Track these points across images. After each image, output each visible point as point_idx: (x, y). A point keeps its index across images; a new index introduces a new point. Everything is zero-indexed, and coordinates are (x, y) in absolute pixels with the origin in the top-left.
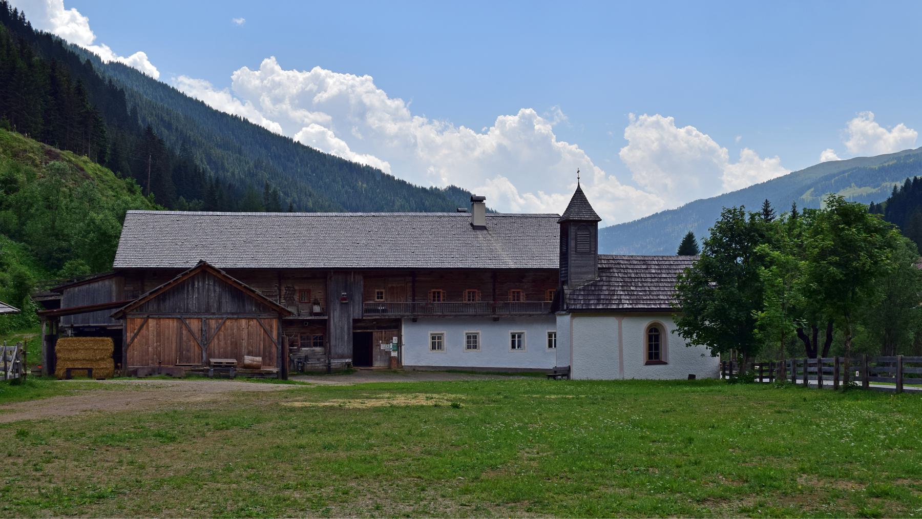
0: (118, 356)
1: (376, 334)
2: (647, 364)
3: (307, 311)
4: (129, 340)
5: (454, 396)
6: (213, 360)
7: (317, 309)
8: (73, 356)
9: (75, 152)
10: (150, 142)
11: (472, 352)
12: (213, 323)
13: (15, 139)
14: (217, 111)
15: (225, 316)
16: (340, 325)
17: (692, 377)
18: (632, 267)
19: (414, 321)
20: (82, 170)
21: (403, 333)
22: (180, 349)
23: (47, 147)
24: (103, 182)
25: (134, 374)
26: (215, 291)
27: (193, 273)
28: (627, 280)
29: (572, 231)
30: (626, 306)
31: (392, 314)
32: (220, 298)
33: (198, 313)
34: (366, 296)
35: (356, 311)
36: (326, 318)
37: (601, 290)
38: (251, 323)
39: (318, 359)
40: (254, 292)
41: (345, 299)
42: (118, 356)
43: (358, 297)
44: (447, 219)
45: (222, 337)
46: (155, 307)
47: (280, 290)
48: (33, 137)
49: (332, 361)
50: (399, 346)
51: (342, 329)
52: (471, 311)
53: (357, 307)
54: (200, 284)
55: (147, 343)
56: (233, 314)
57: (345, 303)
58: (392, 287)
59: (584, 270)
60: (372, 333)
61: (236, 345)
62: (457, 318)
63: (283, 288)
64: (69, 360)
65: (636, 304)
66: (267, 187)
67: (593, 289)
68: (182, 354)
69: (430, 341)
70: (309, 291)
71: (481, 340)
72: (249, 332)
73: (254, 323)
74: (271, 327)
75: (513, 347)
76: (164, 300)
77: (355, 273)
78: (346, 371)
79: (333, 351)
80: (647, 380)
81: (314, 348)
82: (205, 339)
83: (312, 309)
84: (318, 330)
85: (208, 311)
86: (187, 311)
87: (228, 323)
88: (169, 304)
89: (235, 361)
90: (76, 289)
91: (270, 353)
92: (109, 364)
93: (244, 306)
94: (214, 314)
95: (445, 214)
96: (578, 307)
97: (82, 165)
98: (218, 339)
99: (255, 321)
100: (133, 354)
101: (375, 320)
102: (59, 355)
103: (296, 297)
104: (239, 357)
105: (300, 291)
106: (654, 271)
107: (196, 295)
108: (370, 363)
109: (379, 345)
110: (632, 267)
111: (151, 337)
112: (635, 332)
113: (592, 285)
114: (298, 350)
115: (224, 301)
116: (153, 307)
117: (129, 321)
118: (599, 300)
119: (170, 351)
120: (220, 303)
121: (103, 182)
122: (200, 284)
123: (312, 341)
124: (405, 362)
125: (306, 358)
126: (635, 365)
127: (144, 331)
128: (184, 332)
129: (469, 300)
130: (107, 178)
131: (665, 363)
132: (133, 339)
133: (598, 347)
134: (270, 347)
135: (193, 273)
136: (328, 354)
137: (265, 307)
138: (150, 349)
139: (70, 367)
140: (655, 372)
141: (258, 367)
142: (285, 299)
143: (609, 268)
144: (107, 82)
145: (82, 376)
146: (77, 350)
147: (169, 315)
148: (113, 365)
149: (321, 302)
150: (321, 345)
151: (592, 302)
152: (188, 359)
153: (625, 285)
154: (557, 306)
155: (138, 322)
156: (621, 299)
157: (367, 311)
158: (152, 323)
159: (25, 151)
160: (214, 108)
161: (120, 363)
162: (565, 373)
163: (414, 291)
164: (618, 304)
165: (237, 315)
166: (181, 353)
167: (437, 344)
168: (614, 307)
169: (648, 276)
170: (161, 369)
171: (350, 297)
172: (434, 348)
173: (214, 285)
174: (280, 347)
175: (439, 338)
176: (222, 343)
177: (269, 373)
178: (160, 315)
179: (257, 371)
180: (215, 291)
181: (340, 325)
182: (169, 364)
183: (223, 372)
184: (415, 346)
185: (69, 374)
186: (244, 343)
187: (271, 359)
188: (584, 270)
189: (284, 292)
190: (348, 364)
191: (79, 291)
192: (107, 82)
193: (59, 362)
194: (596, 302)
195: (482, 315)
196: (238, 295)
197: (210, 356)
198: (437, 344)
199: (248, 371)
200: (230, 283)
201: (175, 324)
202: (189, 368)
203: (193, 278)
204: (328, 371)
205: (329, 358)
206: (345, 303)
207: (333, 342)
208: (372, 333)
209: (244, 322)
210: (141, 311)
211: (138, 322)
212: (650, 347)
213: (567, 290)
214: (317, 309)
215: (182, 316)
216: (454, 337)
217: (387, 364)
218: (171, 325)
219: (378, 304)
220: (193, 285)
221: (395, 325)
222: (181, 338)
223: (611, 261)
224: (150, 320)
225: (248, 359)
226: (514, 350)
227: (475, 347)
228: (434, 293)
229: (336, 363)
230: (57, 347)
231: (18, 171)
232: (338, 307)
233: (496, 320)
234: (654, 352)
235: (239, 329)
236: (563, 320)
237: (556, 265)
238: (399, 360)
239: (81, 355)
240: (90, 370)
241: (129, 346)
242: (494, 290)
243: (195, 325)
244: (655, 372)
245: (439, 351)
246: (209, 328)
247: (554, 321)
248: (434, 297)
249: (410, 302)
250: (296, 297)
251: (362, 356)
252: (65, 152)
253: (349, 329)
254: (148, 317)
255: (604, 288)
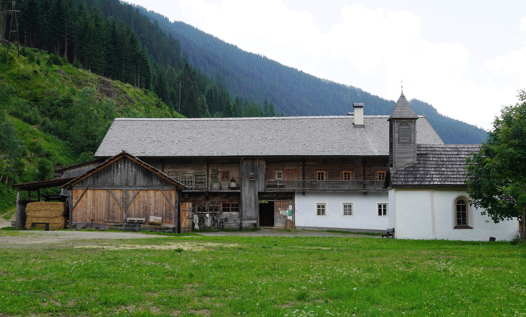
0: (67, 214)
1: (277, 203)
2: (455, 228)
3: (227, 186)
4: (74, 204)
5: (217, 244)
6: (128, 219)
7: (233, 185)
8: (38, 214)
9: (122, 81)
10: (189, 74)
11: (348, 217)
12: (131, 194)
13: (81, 73)
14: (245, 52)
15: (139, 188)
16: (249, 196)
17: (492, 239)
18: (446, 153)
19: (304, 193)
20: (125, 93)
21: (296, 203)
22: (108, 211)
23: (103, 78)
24: (139, 100)
25: (74, 227)
26: (132, 171)
27: (116, 159)
28: (439, 163)
29: (396, 125)
30: (436, 183)
31: (288, 189)
32: (135, 176)
33: (121, 186)
34: (268, 175)
35: (261, 187)
36: (239, 191)
37: (418, 171)
38: (157, 193)
39: (235, 221)
40: (158, 171)
41: (252, 178)
42: (67, 214)
43: (262, 177)
44: (336, 120)
45: (137, 203)
46: (92, 182)
47: (208, 172)
48: (93, 71)
49: (243, 222)
50: (293, 212)
51: (251, 199)
52: (346, 187)
53: (261, 183)
54: (122, 166)
55: (86, 206)
56: (144, 187)
57: (253, 180)
58: (289, 170)
59: (405, 155)
60: (273, 202)
61: (146, 208)
62: (336, 192)
63: (210, 170)
64: (34, 217)
65: (444, 181)
66: (266, 102)
67: (412, 170)
68: (110, 215)
69: (316, 209)
70: (228, 172)
71: (354, 208)
72: (155, 201)
73: (159, 193)
74: (171, 196)
75: (380, 214)
76: (98, 177)
77: (259, 159)
78: (254, 229)
79: (244, 215)
80: (460, 241)
81: (232, 213)
82: (126, 205)
83: (229, 185)
84: (233, 200)
85: (127, 185)
86: (113, 185)
87: (141, 193)
88: (101, 180)
89: (144, 219)
90: (72, 171)
91: (170, 214)
92: (61, 221)
93: (152, 181)
94: (131, 187)
95: (336, 117)
96: (400, 183)
97: (125, 89)
98: (134, 204)
99: (160, 192)
100: (77, 215)
101: (275, 193)
102: (27, 214)
103: (219, 177)
104: (147, 218)
105: (222, 172)
106: (463, 156)
107: (119, 174)
108: (272, 224)
109: (279, 211)
110: (446, 153)
111: (88, 202)
112: (446, 202)
113: (411, 167)
114: (221, 214)
115: (138, 178)
116: (90, 181)
117: (74, 191)
118: (415, 178)
119: (102, 212)
120: (135, 179)
121: (139, 100)
122: (122, 166)
123: (230, 208)
124: (299, 223)
125: (226, 220)
126: (444, 228)
127: (84, 198)
128: (111, 199)
129: (345, 179)
130: (142, 98)
131: (471, 228)
132: (77, 204)
133: (418, 215)
134: (170, 210)
135: (116, 159)
136: (241, 216)
137: (166, 182)
138: (88, 211)
139: (35, 222)
140: (463, 235)
141: (159, 225)
142: (211, 177)
143: (427, 154)
144: (168, 35)
145: (40, 229)
146: (40, 210)
147: (100, 187)
148: (63, 221)
149: (237, 180)
150: (237, 210)
151: (410, 180)
152: (114, 218)
153: (438, 166)
154: (388, 184)
155: (81, 192)
156: (432, 178)
157: (268, 186)
158: (89, 193)
159: (87, 81)
160: (244, 50)
161: (68, 221)
162: (390, 234)
163: (304, 172)
164: (430, 181)
165: (147, 188)
166: (109, 214)
167: (321, 210)
168: (427, 183)
169: (458, 159)
170: (92, 225)
171: (256, 176)
172: (319, 214)
173: (132, 167)
174: (177, 210)
175: (323, 206)
176: (137, 207)
177: (167, 228)
178: (95, 187)
179: (158, 227)
180: (132, 171)
181: (249, 196)
182: (100, 221)
183: (132, 227)
184: (305, 212)
185: (34, 226)
186: (152, 207)
187: (170, 219)
188: (405, 155)
189: (210, 173)
190: (255, 225)
191: (74, 172)
192: (168, 35)
193: (28, 218)
194: (413, 179)
195: (354, 190)
196: (148, 174)
197: (128, 216)
198: (321, 210)
199: (153, 226)
200: (142, 165)
201: (105, 194)
202: (114, 224)
203: (117, 162)
204: (241, 229)
205: (242, 220)
206: (253, 180)
207: (244, 209)
208: (273, 202)
209: (152, 193)
210: (82, 184)
211: (81, 192)
212: (458, 215)
213: (392, 171)
214: (233, 185)
215: (111, 187)
216: (334, 205)
217: (284, 225)
218: (102, 195)
219: (276, 181)
220: (117, 167)
221: (290, 196)
222: (109, 203)
223: (428, 149)
224: (88, 190)
225: (152, 219)
226: (380, 217)
227: (350, 214)
228: (319, 174)
229: (246, 223)
230: (27, 209)
231: (74, 94)
232: (247, 184)
233: (365, 194)
234: (462, 220)
235: (148, 197)
236: (392, 193)
237: (386, 152)
238: (293, 222)
239: (41, 214)
240: (47, 224)
241: (74, 208)
242: (364, 171)
243: (118, 194)
244: (463, 235)
245: (323, 216)
246: (128, 197)
247: (387, 194)
248: (319, 176)
249: (301, 179)
250: (219, 177)
251: (266, 217)
252: (114, 82)
253: (255, 199)
254: (87, 189)
255: (421, 169)
